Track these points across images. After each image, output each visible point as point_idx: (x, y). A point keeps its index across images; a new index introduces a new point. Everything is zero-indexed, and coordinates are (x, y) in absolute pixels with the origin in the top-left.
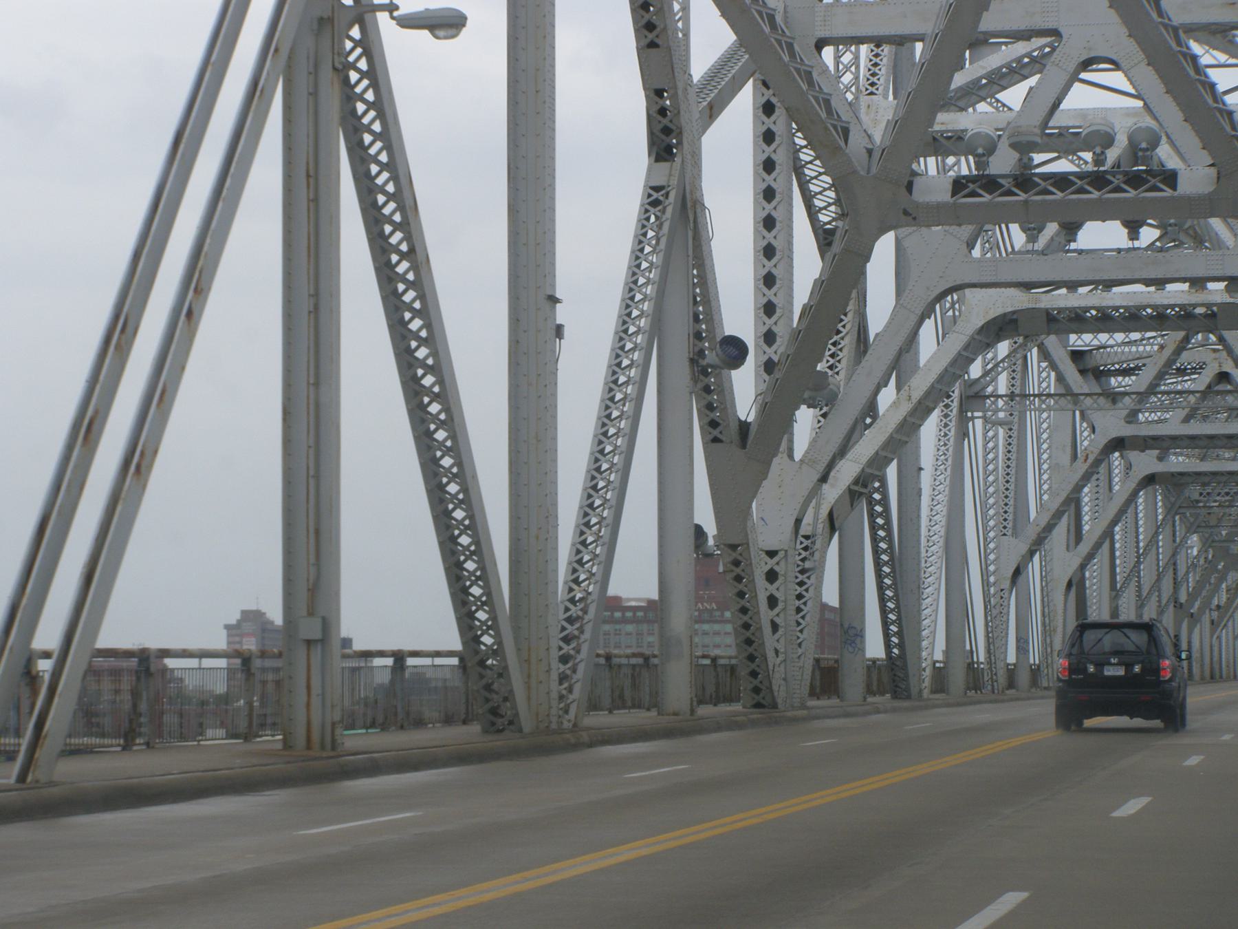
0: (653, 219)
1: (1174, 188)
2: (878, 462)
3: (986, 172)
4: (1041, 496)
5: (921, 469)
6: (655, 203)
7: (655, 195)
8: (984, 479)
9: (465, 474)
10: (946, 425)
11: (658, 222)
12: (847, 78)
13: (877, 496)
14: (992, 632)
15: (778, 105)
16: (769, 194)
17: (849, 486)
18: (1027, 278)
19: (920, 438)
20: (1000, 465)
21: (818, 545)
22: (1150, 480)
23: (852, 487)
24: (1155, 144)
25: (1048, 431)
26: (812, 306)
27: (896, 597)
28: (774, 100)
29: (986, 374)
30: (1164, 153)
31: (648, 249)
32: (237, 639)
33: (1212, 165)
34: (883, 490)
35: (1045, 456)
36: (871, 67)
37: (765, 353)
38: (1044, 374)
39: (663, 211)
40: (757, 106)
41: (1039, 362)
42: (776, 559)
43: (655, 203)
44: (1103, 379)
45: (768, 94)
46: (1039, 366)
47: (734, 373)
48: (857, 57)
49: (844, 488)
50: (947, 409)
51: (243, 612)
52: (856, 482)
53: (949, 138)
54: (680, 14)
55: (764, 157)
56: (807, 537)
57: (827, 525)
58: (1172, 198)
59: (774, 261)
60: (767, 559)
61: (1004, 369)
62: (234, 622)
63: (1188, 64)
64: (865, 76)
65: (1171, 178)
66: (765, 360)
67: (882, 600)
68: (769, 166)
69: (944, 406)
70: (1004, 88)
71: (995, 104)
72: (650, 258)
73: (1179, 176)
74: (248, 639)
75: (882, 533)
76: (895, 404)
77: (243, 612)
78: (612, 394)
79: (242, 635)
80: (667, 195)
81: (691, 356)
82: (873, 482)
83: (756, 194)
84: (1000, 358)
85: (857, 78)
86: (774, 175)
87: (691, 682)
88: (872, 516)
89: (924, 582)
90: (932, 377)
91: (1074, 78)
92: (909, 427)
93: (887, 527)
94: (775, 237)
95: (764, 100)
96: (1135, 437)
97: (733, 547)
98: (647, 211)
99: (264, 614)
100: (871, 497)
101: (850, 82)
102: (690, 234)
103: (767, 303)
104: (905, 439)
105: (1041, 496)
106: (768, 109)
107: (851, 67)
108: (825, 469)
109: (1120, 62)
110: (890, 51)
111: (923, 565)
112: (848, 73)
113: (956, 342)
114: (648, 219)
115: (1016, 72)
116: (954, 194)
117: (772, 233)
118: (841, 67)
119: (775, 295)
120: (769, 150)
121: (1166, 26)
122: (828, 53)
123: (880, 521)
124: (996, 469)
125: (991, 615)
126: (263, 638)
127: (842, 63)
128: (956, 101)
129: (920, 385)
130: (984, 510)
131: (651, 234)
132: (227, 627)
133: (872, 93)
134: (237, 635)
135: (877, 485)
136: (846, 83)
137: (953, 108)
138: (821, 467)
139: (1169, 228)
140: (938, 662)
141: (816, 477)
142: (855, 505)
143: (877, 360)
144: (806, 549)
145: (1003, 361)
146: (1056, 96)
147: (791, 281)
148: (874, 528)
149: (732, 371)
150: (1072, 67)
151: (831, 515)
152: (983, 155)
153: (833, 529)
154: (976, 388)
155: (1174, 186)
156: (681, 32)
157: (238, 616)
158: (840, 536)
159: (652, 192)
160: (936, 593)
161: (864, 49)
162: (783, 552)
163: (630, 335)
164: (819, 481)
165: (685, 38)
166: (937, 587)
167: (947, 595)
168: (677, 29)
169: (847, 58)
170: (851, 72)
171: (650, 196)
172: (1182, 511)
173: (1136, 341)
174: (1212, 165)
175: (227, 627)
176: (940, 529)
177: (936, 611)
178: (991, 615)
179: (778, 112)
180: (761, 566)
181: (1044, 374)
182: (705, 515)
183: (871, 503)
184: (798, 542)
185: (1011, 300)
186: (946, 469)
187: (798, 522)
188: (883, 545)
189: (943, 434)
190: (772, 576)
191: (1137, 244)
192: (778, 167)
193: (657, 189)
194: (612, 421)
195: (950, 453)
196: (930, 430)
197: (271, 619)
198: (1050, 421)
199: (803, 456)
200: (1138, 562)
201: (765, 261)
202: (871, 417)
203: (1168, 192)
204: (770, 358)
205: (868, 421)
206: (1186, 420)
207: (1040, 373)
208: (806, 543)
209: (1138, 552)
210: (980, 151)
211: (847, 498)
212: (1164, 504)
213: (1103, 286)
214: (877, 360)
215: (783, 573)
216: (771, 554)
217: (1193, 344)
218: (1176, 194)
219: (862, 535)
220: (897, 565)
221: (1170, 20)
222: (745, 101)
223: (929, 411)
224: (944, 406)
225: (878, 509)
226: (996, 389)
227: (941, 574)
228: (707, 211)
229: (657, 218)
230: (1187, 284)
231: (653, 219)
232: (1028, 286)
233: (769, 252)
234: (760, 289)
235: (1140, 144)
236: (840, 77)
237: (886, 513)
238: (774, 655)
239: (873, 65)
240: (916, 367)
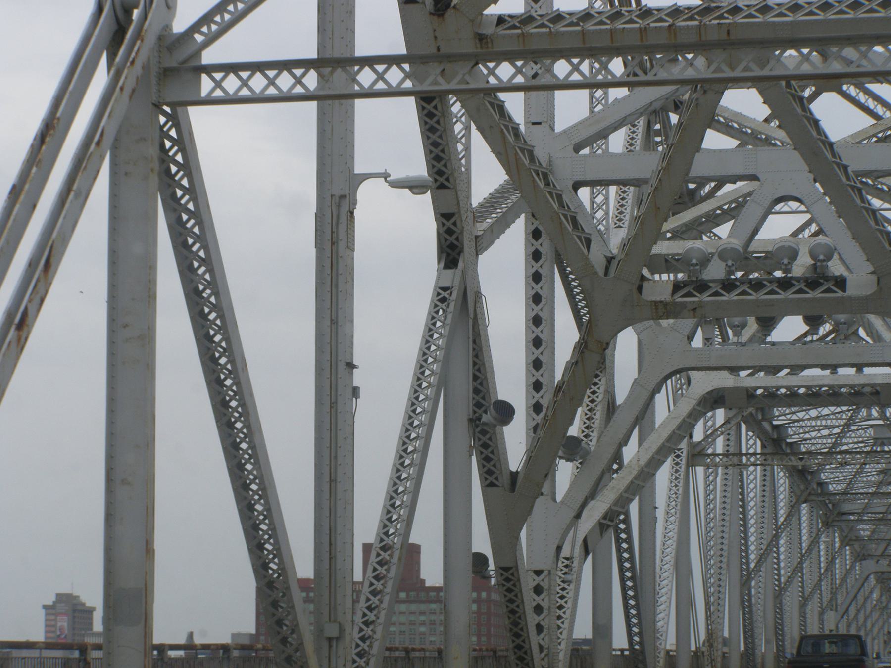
0: (441, 312)
1: (844, 290)
2: (623, 502)
5: (656, 508)
6: (443, 300)
8: (705, 526)
9: (277, 532)
10: (677, 471)
11: (444, 315)
12: (600, 214)
13: (622, 526)
14: (711, 625)
15: (543, 231)
16: (536, 277)
17: (599, 520)
19: (655, 407)
20: (718, 512)
21: (576, 564)
23: (603, 521)
24: (829, 258)
25: (755, 508)
27: (639, 624)
28: (541, 228)
29: (707, 437)
30: (836, 268)
31: (439, 324)
32: (53, 617)
33: (872, 273)
34: (627, 521)
36: (617, 215)
37: (533, 288)
38: (751, 442)
39: (448, 306)
40: (529, 362)
41: (747, 432)
42: (542, 576)
43: (443, 300)
45: (536, 223)
46: (747, 435)
47: (505, 428)
48: (607, 198)
49: (595, 521)
50: (677, 462)
51: (58, 595)
52: (605, 517)
53: (678, 260)
54: (464, 153)
55: (533, 270)
56: (567, 559)
57: (583, 549)
58: (843, 298)
59: (540, 350)
60: (535, 577)
61: (722, 433)
62: (51, 603)
63: (855, 194)
64: (614, 214)
65: (841, 283)
66: (533, 359)
67: (628, 617)
68: (536, 256)
69: (676, 456)
70: (718, 225)
71: (713, 238)
72: (440, 330)
73: (847, 280)
74: (61, 617)
75: (626, 555)
76: (637, 457)
77: (58, 595)
78: (405, 447)
79: (57, 614)
81: (471, 417)
82: (618, 515)
83: (527, 299)
84: (718, 425)
85: (607, 213)
86: (540, 284)
87: (469, 662)
88: (618, 541)
89: (658, 593)
90: (665, 434)
91: (769, 212)
92: (647, 474)
93: (630, 550)
94: (542, 375)
95: (533, 228)
97: (506, 569)
98: (436, 306)
99: (78, 597)
100: (617, 526)
101: (602, 217)
103: (536, 381)
104: (642, 484)
106: (536, 234)
107: (602, 206)
108: (580, 508)
109: (804, 200)
110: (634, 191)
111: (658, 588)
112: (600, 210)
113: (686, 407)
114: (437, 312)
115: (727, 214)
117: (539, 393)
118: (595, 206)
119: (543, 600)
120: (536, 266)
121: (838, 164)
122: (584, 193)
123: (626, 555)
125: (710, 620)
126: (74, 617)
127: (596, 203)
128: (681, 234)
129: (655, 441)
130: (706, 551)
132: (45, 607)
134: (53, 614)
135: (622, 517)
136: (599, 203)
137: (678, 238)
139: (841, 326)
140: (671, 651)
141: (573, 514)
142: (603, 535)
143: (622, 419)
144: (566, 566)
145: (721, 426)
146: (755, 225)
147: (553, 342)
148: (619, 550)
149: (504, 427)
150: (767, 204)
151: (585, 541)
153: (587, 552)
154: (698, 449)
155: (844, 289)
156: (464, 167)
157: (54, 599)
158: (593, 558)
160: (666, 617)
161: (613, 189)
162: (547, 571)
163: (420, 402)
164: (574, 517)
165: (466, 172)
166: (670, 588)
167: (677, 602)
168: (461, 165)
169: (600, 199)
170: (603, 210)
171: (439, 294)
172: (851, 543)
173: (825, 436)
174: (872, 273)
175: (45, 607)
176: (671, 550)
177: (668, 615)
178: (710, 620)
179: (544, 236)
180: (528, 582)
181: (751, 442)
182: (481, 543)
183: (617, 531)
184: (560, 562)
185: (723, 380)
186: (676, 505)
187: (559, 549)
188: (627, 565)
189: (674, 478)
190: (538, 590)
192: (543, 322)
193: (445, 289)
194: (405, 467)
195: (679, 500)
196: (663, 476)
197: (83, 601)
198: (756, 500)
199: (563, 498)
200: (820, 580)
201: (534, 393)
202: (617, 463)
203: (840, 294)
204: (537, 249)
205: (615, 466)
207: (748, 441)
208: (566, 562)
209: (820, 572)
211: (598, 531)
212: (840, 538)
214: (622, 419)
215: (547, 646)
216: (538, 573)
217: (860, 419)
218: (845, 295)
219: (611, 554)
220: (639, 589)
221: (841, 160)
222: (518, 229)
223: (661, 463)
224: (676, 456)
225: (623, 536)
226: (715, 449)
227: (671, 595)
228: (483, 297)
229: (443, 311)
230: (855, 369)
231: (441, 312)
233: (537, 343)
234: (529, 327)
235: (818, 257)
236: (595, 213)
237: (629, 540)
238: (538, 650)
239: (619, 213)
240: (653, 428)
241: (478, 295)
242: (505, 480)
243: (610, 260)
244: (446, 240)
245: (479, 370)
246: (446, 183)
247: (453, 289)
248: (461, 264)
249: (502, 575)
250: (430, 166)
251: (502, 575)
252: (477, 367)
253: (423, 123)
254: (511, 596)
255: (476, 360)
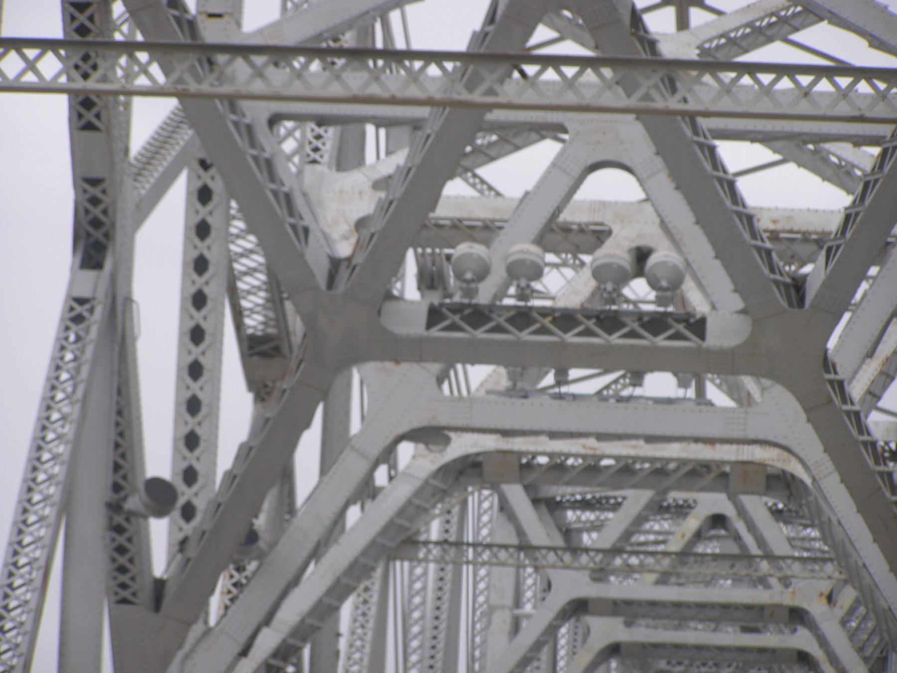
3: (474, 301)
4: (474, 636)
6: (78, 319)
7: (79, 309)
18: (507, 426)
22: (614, 650)
26: (251, 449)
30: (698, 303)
35: (482, 586)
43: (78, 319)
44: (557, 513)
65: (699, 327)
80: (91, 311)
96: (601, 601)
97: (94, 182)
98: (67, 328)
102: (117, 347)
105: (474, 636)
116: (430, 324)
124: (424, 588)
131: (64, 376)
133: (314, 162)
138: (243, 639)
141: (238, 649)
152: (473, 281)
159: (75, 305)
171: (72, 309)
191: (638, 392)
193: (81, 301)
203: (693, 342)
206: (658, 582)
210: (469, 276)
213: (734, 580)
232: (505, 433)
241: (129, 300)
242: (146, 594)
243: (335, 264)
244: (87, 211)
245: (123, 456)
246: (95, 121)
247: (95, 303)
248: (108, 264)
249: (85, 191)
250: (69, 18)
251: (85, 191)
252: (120, 451)
253: (68, 19)
254: (124, 578)
255: (120, 419)
